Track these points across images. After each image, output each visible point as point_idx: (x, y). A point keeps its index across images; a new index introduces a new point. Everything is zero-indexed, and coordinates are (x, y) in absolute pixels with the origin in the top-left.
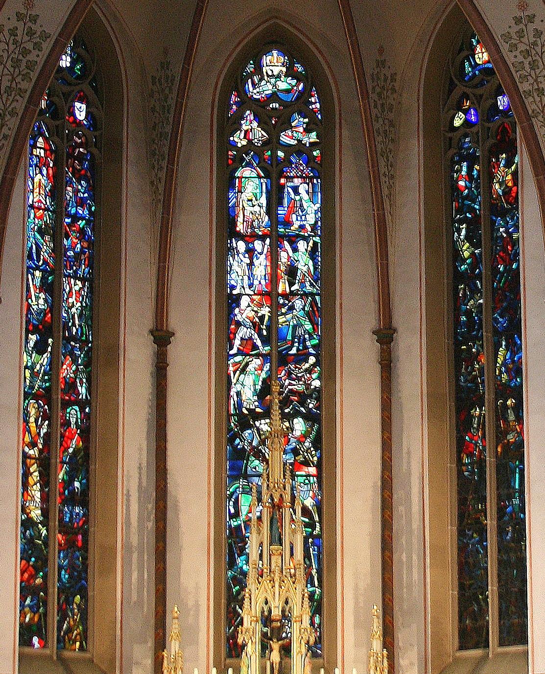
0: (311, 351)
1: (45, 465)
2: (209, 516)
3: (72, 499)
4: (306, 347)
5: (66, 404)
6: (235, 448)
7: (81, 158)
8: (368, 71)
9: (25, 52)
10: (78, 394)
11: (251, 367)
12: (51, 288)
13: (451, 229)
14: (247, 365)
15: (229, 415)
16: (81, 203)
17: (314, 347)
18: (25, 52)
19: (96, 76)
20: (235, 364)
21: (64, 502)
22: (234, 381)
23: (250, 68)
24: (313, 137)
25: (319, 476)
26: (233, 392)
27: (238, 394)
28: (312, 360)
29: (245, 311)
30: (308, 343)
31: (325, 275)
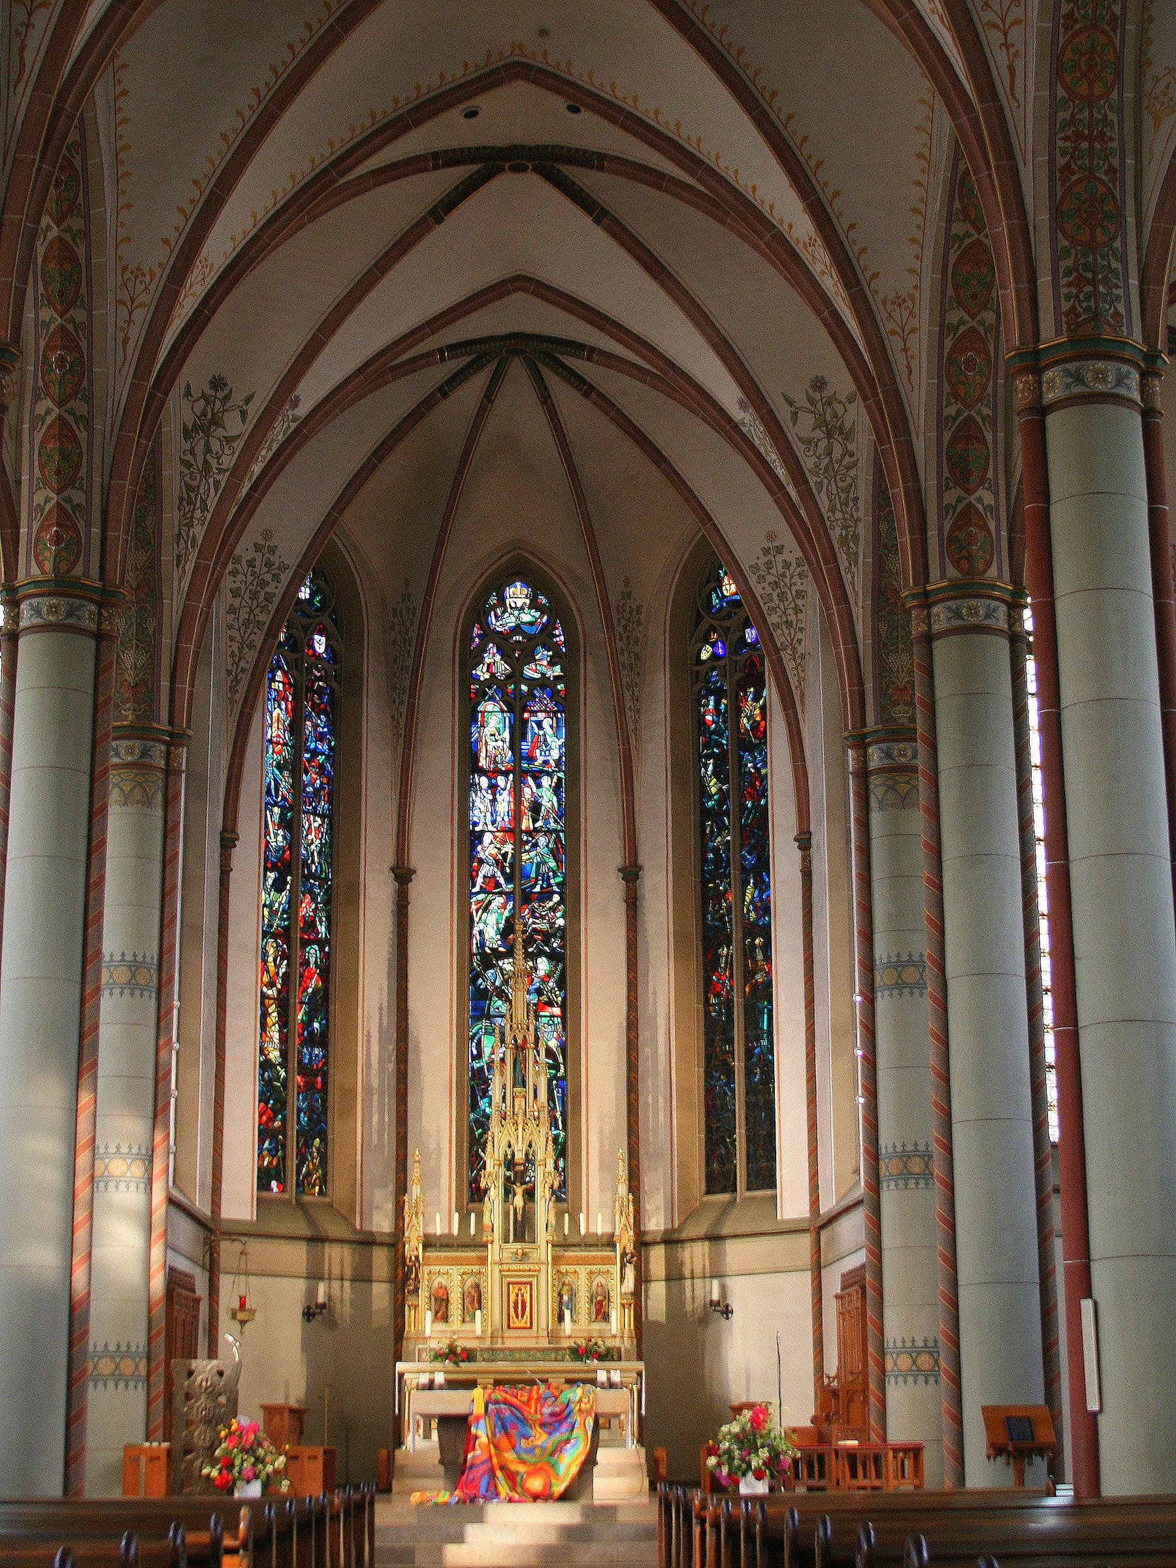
0: (555, 889)
1: (284, 1005)
2: (451, 1058)
3: (311, 1040)
4: (550, 885)
5: (305, 944)
6: (477, 988)
9: (264, 584)
10: (318, 933)
11: (493, 906)
12: (289, 825)
13: (699, 764)
14: (490, 903)
15: (472, 955)
16: (321, 737)
17: (558, 884)
18: (264, 584)
19: (336, 609)
20: (478, 902)
21: (304, 1043)
22: (476, 919)
23: (493, 600)
24: (557, 670)
25: (563, 1017)
26: (475, 931)
27: (481, 933)
28: (556, 898)
29: (488, 849)
30: (552, 881)
31: (570, 811)
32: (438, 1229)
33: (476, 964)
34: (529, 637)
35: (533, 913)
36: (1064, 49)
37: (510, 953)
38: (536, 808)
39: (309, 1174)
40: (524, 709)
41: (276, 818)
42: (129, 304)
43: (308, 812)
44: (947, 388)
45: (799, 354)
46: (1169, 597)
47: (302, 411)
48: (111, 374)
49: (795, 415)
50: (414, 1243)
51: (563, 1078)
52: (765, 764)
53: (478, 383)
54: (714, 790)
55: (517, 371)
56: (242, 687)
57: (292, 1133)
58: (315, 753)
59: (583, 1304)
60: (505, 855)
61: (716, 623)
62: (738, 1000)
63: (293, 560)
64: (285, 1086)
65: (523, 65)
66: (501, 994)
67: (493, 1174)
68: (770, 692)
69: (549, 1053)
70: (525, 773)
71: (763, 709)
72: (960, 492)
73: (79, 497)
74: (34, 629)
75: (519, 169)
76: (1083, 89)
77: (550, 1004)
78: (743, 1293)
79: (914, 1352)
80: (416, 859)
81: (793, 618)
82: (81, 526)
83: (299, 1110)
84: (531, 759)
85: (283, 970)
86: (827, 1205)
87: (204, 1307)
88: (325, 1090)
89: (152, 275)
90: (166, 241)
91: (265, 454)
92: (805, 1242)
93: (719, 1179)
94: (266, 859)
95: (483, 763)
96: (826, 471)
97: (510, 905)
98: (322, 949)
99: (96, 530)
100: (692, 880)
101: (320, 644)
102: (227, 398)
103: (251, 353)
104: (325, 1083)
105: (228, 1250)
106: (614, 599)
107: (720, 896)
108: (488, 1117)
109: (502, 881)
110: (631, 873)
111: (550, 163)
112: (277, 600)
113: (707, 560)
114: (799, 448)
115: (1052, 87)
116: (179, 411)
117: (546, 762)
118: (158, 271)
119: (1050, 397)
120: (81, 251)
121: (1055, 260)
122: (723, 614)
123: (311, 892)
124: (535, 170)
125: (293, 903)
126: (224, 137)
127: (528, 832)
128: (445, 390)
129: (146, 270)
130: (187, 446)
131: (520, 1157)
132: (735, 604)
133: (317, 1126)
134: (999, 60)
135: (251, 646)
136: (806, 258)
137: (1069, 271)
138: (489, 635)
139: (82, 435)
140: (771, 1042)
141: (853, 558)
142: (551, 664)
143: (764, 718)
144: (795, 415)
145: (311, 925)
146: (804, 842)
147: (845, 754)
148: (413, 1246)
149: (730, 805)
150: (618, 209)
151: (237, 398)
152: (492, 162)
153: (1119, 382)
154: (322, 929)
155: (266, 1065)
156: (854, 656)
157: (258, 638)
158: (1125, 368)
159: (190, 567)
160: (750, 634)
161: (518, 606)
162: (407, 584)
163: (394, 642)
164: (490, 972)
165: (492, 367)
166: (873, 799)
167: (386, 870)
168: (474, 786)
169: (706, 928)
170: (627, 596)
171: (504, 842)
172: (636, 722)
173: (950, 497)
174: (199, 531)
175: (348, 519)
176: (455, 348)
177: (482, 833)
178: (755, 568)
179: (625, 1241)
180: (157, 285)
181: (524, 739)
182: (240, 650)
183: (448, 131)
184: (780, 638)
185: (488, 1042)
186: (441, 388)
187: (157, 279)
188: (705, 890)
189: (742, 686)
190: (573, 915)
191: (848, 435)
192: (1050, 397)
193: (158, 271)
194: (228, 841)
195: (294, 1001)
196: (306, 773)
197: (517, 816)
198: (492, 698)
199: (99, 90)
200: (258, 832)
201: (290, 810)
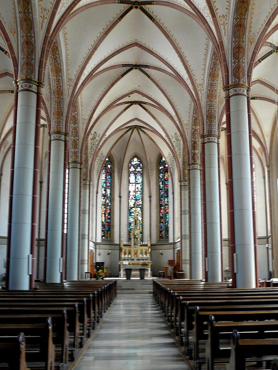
1: (105, 214)
3: (109, 219)
7: (109, 173)
8: (148, 161)
9: (101, 159)
12: (105, 190)
13: (159, 182)
16: (109, 179)
18: (101, 159)
19: (111, 161)
23: (132, 160)
24: (141, 170)
29: (132, 194)
31: (142, 189)
34: (137, 165)
42: (43, 17)
45: (172, 130)
46: (250, 113)
47: (107, 136)
48: (39, 31)
53: (130, 131)
55: (135, 130)
63: (105, 155)
65: (136, 91)
66: (133, 213)
73: (77, 150)
74: (54, 140)
75: (136, 104)
76: (211, 100)
79: (186, 263)
80: (122, 195)
82: (77, 154)
87: (94, 254)
89: (49, 11)
90: (88, 115)
91: (102, 142)
101: (109, 166)
102: (96, 135)
103: (99, 129)
106: (148, 161)
111: (140, 103)
113: (160, 156)
114: (173, 142)
116: (90, 137)
118: (74, 79)
119: (205, 141)
120: (76, 117)
125: (106, 201)
126: (96, 101)
128: (126, 133)
129: (47, 9)
130: (91, 141)
134: (200, 95)
136: (174, 118)
138: (132, 165)
139: (77, 141)
146: (173, 193)
148: (122, 246)
150: (149, 110)
151: (98, 135)
152: (132, 103)
153: (214, 140)
157: (101, 166)
158: (215, 138)
159: (92, 157)
161: (135, 161)
165: (131, 130)
174: (93, 153)
175: (113, 150)
180: (87, 121)
186: (125, 133)
187: (50, 12)
191: (180, 141)
192: (231, 95)
193: (74, 79)
194: (97, 193)
199: (79, 97)
200: (101, 191)
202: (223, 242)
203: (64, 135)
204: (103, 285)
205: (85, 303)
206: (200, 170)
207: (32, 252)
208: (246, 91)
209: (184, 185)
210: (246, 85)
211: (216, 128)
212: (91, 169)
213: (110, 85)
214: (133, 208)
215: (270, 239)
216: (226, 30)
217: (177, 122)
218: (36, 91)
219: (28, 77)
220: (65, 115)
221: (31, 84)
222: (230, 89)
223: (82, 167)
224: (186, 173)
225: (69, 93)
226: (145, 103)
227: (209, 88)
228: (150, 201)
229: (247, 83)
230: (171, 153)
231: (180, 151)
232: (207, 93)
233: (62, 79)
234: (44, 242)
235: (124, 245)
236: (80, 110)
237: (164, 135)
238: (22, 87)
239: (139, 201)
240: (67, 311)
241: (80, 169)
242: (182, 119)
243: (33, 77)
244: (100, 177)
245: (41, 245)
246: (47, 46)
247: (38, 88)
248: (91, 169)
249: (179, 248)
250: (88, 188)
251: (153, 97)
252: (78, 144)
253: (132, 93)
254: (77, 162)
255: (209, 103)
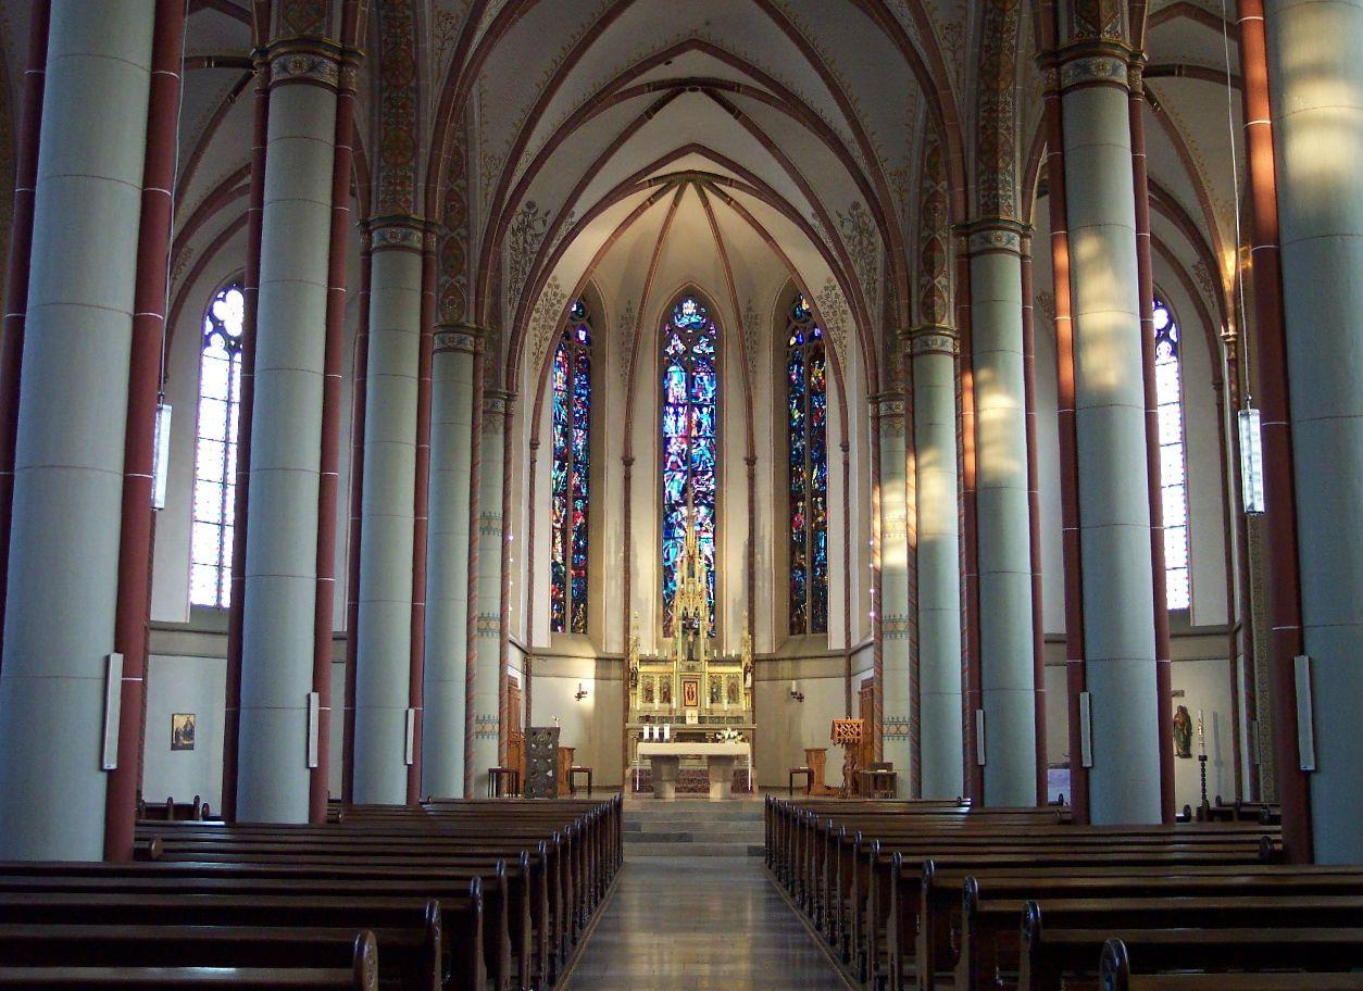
3: (578, 551)
5: (575, 499)
7: (583, 362)
9: (552, 305)
12: (565, 435)
16: (583, 387)
17: (712, 467)
18: (552, 305)
23: (676, 310)
26: (667, 492)
28: (710, 474)
29: (673, 448)
32: (647, 653)
33: (666, 510)
35: (697, 482)
36: (985, 64)
37: (685, 504)
38: (699, 424)
39: (578, 622)
40: (693, 370)
41: (559, 431)
43: (576, 428)
44: (923, 222)
47: (576, 219)
49: (842, 223)
50: (635, 661)
51: (714, 572)
52: (824, 404)
54: (796, 417)
55: (690, 189)
56: (541, 362)
57: (569, 601)
58: (580, 395)
59: (724, 693)
60: (683, 450)
61: (799, 325)
62: (808, 531)
64: (565, 576)
65: (696, 40)
66: (680, 526)
67: (677, 624)
68: (827, 364)
69: (707, 558)
70: (694, 405)
71: (823, 373)
72: (928, 278)
77: (707, 531)
78: (809, 687)
80: (635, 453)
81: (840, 325)
83: (573, 588)
84: (697, 398)
85: (563, 513)
86: (855, 642)
88: (586, 577)
91: (556, 242)
92: (842, 662)
93: (796, 627)
94: (555, 454)
95: (671, 400)
96: (859, 252)
97: (685, 477)
98: (584, 502)
99: (473, 298)
100: (784, 466)
101: (582, 335)
104: (586, 573)
105: (535, 662)
106: (743, 311)
107: (799, 475)
108: (674, 592)
109: (680, 463)
110: (751, 461)
112: (559, 314)
115: (979, 83)
117: (705, 400)
120: (462, 149)
121: (978, 176)
122: (803, 319)
123: (578, 471)
124: (703, 90)
125: (567, 479)
127: (695, 438)
128: (651, 200)
131: (691, 615)
132: (808, 313)
133: (582, 597)
135: (546, 339)
137: (984, 182)
140: (826, 554)
141: (873, 300)
142: (708, 346)
143: (824, 378)
144: (842, 223)
145: (578, 489)
146: (845, 447)
147: (867, 406)
149: (805, 425)
152: (677, 87)
154: (584, 491)
155: (555, 565)
156: (873, 353)
158: (1012, 234)
159: (516, 305)
160: (817, 332)
162: (629, 302)
163: (623, 334)
164: (675, 514)
166: (881, 432)
167: (619, 458)
168: (666, 413)
169: (791, 492)
170: (749, 309)
171: (681, 443)
172: (754, 379)
173: (923, 281)
174: (521, 285)
176: (657, 180)
177: (670, 438)
178: (820, 297)
179: (747, 660)
181: (693, 387)
182: (540, 341)
183: (659, 73)
184: (833, 336)
185: (672, 552)
188: (791, 471)
189: (812, 359)
190: (719, 483)
194: (534, 445)
195: (570, 530)
196: (576, 406)
197: (689, 428)
198: (676, 364)
200: (550, 438)
201: (567, 426)
202: (1043, 646)
203: (422, 227)
204: (522, 842)
205: (505, 886)
206: (955, 357)
207: (318, 683)
208: (1123, 71)
209: (889, 412)
210: (1127, 43)
211: (1014, 193)
212: (512, 352)
213: (594, 24)
214: (679, 505)
215: (1241, 636)
216: (960, 64)
217: (862, 163)
218: (333, 82)
219: (308, 32)
220: (424, 151)
221: (317, 59)
222: (1064, 62)
223: (481, 349)
224: (900, 367)
225: (439, 69)
226: (731, 86)
227: (986, 42)
228: (752, 478)
229: (1128, 40)
230: (835, 282)
231: (870, 265)
232: (980, 60)
233: (415, 14)
234: (343, 645)
235: (645, 661)
236: (477, 125)
237: (806, 210)
238: (284, 68)
239: (706, 477)
240: (444, 913)
241: (476, 354)
242: (880, 154)
243: (324, 32)
244: (548, 382)
245: (345, 651)
246: (449, 121)
247: (340, 71)
248: (512, 352)
249: (870, 674)
250: (501, 429)
251: (762, 65)
252: (469, 254)
253: (680, 49)
254: (462, 326)
255: (986, 99)
